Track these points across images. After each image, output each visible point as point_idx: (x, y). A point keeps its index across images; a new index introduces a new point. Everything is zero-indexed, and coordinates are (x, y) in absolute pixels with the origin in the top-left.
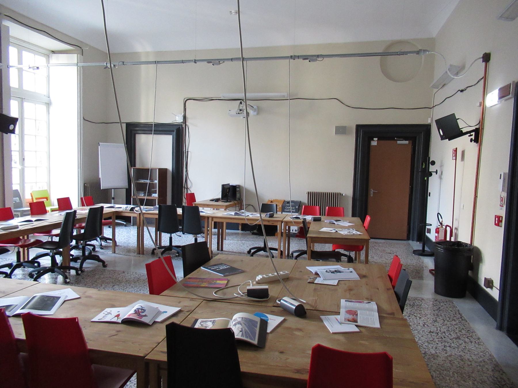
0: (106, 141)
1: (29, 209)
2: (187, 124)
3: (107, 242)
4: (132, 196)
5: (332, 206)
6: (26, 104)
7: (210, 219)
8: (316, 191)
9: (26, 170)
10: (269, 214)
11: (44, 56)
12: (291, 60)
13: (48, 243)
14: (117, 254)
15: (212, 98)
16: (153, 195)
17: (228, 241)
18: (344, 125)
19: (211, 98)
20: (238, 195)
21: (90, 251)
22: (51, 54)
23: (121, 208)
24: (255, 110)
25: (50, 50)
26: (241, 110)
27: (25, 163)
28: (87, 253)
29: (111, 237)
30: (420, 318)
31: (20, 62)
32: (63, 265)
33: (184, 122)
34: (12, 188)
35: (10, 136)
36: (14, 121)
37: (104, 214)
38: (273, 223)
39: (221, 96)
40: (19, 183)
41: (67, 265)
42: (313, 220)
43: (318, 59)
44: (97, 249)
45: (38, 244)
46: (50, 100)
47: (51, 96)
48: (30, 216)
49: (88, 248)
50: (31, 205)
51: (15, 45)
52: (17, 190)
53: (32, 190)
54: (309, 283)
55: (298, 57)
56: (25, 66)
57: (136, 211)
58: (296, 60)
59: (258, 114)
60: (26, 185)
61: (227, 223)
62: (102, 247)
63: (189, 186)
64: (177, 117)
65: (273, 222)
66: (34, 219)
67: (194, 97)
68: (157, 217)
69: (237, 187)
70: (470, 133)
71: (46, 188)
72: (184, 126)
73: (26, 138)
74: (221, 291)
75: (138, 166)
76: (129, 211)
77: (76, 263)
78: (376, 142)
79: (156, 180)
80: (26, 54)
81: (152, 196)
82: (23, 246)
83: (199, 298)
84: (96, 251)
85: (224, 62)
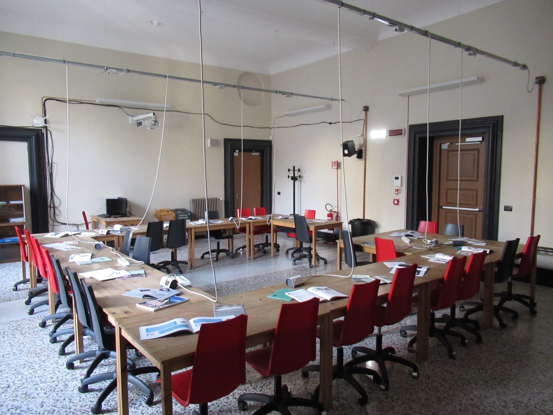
7: (193, 230)
18: (217, 138)
19: (80, 101)
63: (56, 205)
72: (44, 131)
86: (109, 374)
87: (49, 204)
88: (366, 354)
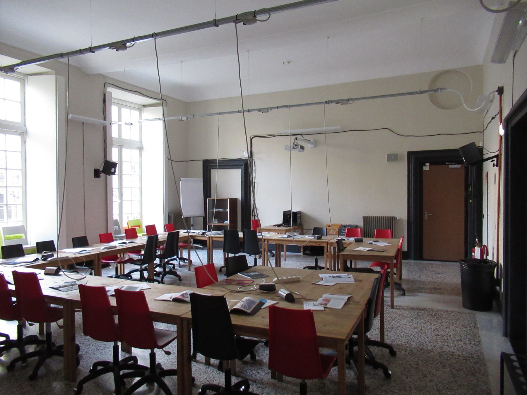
0: (186, 177)
1: (125, 235)
2: (253, 158)
3: (185, 262)
4: (208, 223)
5: (379, 229)
6: (124, 150)
8: (371, 216)
9: (124, 203)
10: (317, 236)
11: (138, 110)
12: (326, 105)
13: (138, 260)
14: (192, 271)
15: (274, 134)
16: (226, 222)
17: (288, 262)
20: (299, 221)
21: (170, 268)
22: (143, 108)
23: (195, 233)
24: (312, 143)
25: (141, 105)
26: (296, 145)
27: (123, 197)
28: (167, 270)
29: (187, 258)
30: (435, 325)
31: (120, 120)
32: (149, 278)
33: (251, 157)
34: (113, 218)
35: (112, 177)
36: (114, 165)
37: (180, 238)
38: (319, 244)
39: (282, 132)
40: (118, 214)
41: (152, 278)
42: (355, 241)
43: (348, 102)
44: (176, 268)
45: (131, 261)
46: (142, 145)
47: (143, 142)
48: (125, 240)
49: (169, 266)
50: (127, 231)
51: (116, 104)
52: (117, 220)
53: (128, 220)
54: (313, 284)
55: (332, 102)
56: (122, 123)
57: (206, 235)
58: (331, 104)
59: (315, 146)
60: (123, 216)
61: (287, 246)
62: (180, 266)
64: (245, 153)
65: (319, 244)
66: (127, 242)
67: (261, 134)
68: (223, 240)
69: (298, 214)
70: (492, 159)
71: (139, 218)
73: (124, 177)
74: (244, 287)
75: (214, 196)
76: (201, 235)
77: (159, 278)
78: (429, 167)
79: (228, 209)
80: (124, 110)
81: (225, 223)
82: (120, 263)
83: (228, 290)
84: (176, 269)
85: (271, 110)
86: (157, 329)
87: (252, 213)
88: (141, 378)
